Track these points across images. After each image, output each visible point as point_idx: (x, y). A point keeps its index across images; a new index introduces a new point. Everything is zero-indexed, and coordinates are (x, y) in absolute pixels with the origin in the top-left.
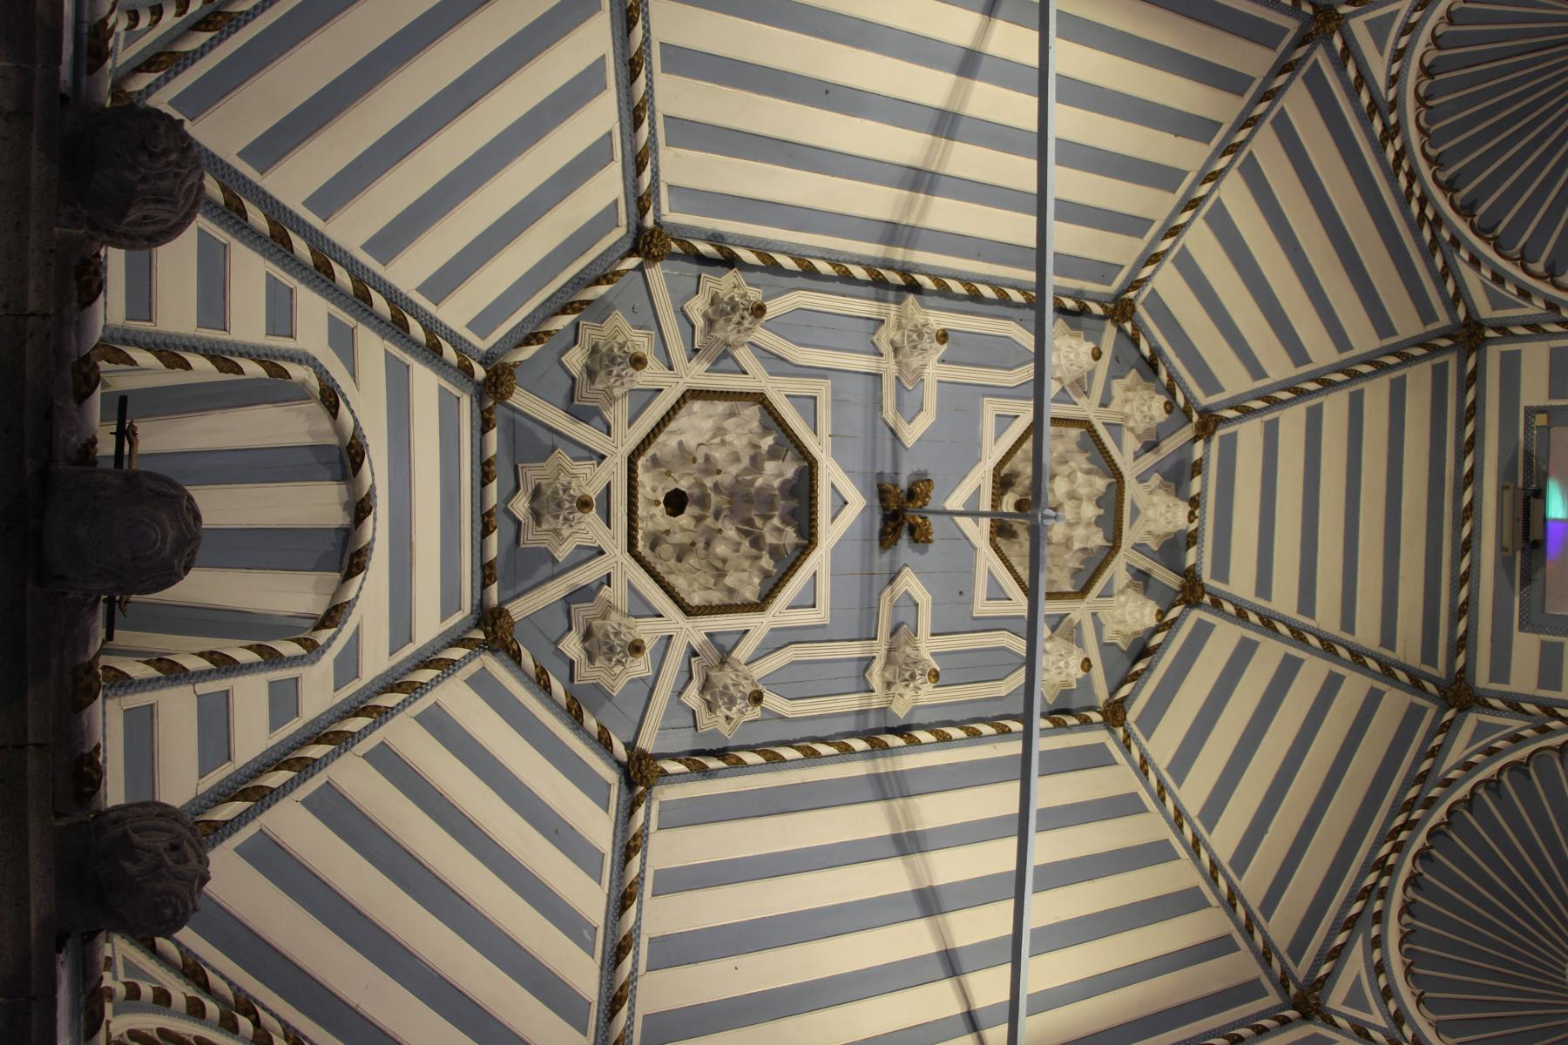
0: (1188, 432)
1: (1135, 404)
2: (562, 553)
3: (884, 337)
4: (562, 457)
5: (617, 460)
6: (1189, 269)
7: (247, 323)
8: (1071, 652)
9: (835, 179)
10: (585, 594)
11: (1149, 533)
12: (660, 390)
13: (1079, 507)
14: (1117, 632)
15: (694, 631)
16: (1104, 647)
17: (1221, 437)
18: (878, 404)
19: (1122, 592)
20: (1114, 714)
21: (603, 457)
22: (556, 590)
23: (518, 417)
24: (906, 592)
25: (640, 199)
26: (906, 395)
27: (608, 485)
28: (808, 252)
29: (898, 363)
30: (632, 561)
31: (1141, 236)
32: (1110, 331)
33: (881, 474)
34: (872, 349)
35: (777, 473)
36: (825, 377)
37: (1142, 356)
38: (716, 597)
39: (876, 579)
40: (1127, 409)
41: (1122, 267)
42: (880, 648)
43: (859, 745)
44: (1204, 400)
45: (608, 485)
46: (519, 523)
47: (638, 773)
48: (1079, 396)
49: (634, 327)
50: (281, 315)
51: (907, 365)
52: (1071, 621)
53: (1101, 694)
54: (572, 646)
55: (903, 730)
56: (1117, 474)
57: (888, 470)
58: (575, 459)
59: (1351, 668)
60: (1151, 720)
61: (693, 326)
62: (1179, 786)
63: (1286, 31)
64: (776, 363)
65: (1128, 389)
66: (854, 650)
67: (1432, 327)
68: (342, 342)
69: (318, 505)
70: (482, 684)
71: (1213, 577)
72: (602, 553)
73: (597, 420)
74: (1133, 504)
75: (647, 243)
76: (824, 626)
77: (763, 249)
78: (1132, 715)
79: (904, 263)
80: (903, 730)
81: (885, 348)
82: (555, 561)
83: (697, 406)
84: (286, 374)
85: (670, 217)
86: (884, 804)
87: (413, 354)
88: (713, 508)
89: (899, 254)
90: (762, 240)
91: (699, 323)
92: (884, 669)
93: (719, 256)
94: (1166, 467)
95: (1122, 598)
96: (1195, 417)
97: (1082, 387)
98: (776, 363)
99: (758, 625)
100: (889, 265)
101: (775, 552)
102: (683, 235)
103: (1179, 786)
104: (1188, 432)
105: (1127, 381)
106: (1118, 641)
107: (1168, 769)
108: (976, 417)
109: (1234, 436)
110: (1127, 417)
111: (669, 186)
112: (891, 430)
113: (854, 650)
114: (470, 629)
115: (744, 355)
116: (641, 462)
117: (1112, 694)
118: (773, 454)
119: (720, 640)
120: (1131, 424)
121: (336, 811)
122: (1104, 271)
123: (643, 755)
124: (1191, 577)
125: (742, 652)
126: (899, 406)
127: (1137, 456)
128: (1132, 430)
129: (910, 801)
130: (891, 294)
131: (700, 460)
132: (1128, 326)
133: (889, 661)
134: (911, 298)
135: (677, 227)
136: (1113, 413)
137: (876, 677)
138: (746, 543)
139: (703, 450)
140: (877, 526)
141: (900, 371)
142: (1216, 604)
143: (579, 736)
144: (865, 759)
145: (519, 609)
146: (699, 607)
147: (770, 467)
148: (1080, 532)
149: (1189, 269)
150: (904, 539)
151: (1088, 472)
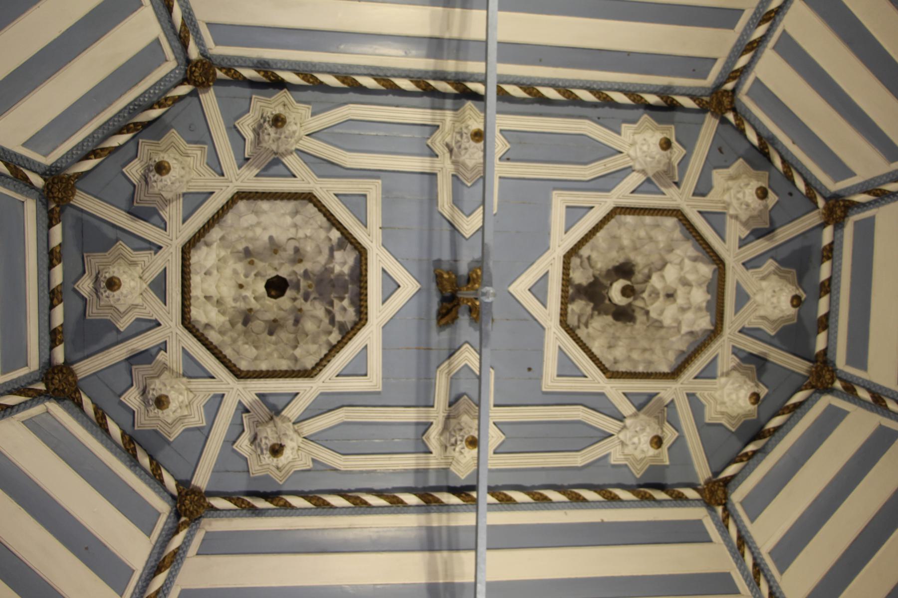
0: (813, 219)
1: (732, 192)
2: (123, 325)
3: (438, 142)
4: (122, 247)
5: (172, 250)
6: (792, 52)
8: (643, 430)
10: (144, 357)
12: (212, 193)
13: (689, 293)
14: (722, 413)
15: (247, 391)
16: (703, 427)
17: (856, 223)
19: (727, 374)
20: (716, 493)
21: (160, 248)
22: (119, 353)
23: (85, 216)
24: (466, 365)
25: (180, 37)
26: (466, 191)
28: (351, 71)
29: (455, 163)
30: (186, 332)
31: (732, 27)
32: (710, 124)
34: (427, 151)
35: (343, 263)
36: (378, 178)
37: (752, 145)
38: (284, 365)
39: (434, 355)
40: (726, 198)
41: (715, 60)
42: (438, 414)
43: (411, 499)
44: (834, 186)
46: (84, 300)
47: (189, 505)
48: (668, 186)
49: (189, 142)
51: (464, 165)
52: (661, 399)
53: (703, 472)
54: (132, 398)
55: (464, 491)
56: (718, 262)
57: (446, 256)
58: (135, 250)
60: (758, 503)
61: (245, 140)
62: (782, 572)
64: (325, 167)
65: (732, 178)
66: (411, 415)
71: (849, 362)
72: (159, 325)
73: (156, 219)
75: (200, 73)
76: (378, 393)
77: (306, 72)
78: (737, 496)
79: (457, 73)
80: (464, 491)
81: (439, 148)
82: (118, 331)
83: (242, 205)
85: (216, 50)
86: (427, 555)
88: (302, 291)
89: (450, 66)
90: (306, 64)
91: (249, 136)
92: (441, 434)
93: (264, 79)
94: (784, 253)
95: (723, 380)
96: (821, 203)
97: (672, 177)
98: (325, 167)
99: (308, 390)
100: (441, 76)
101: (342, 327)
103: (782, 572)
105: (731, 170)
106: (724, 422)
107: (771, 553)
110: (728, 205)
111: (208, 24)
112: (449, 222)
113: (411, 415)
114: (36, 381)
115: (293, 162)
116: (575, 261)
117: (716, 474)
118: (341, 246)
119: (271, 400)
120: (731, 211)
122: (697, 65)
123: (196, 491)
124: (823, 364)
125: (293, 411)
126: (456, 201)
128: (736, 217)
129: (455, 555)
130: (449, 102)
131: (291, 252)
132: (730, 116)
133: (446, 428)
134: (469, 104)
135: (223, 57)
136: (712, 201)
137: (433, 437)
138: (326, 321)
139: (293, 244)
141: (457, 170)
142: (849, 390)
143: (135, 472)
144: (418, 512)
145: (84, 369)
147: (338, 255)
148: (689, 315)
149: (792, 52)
150: (464, 320)
151: (695, 260)
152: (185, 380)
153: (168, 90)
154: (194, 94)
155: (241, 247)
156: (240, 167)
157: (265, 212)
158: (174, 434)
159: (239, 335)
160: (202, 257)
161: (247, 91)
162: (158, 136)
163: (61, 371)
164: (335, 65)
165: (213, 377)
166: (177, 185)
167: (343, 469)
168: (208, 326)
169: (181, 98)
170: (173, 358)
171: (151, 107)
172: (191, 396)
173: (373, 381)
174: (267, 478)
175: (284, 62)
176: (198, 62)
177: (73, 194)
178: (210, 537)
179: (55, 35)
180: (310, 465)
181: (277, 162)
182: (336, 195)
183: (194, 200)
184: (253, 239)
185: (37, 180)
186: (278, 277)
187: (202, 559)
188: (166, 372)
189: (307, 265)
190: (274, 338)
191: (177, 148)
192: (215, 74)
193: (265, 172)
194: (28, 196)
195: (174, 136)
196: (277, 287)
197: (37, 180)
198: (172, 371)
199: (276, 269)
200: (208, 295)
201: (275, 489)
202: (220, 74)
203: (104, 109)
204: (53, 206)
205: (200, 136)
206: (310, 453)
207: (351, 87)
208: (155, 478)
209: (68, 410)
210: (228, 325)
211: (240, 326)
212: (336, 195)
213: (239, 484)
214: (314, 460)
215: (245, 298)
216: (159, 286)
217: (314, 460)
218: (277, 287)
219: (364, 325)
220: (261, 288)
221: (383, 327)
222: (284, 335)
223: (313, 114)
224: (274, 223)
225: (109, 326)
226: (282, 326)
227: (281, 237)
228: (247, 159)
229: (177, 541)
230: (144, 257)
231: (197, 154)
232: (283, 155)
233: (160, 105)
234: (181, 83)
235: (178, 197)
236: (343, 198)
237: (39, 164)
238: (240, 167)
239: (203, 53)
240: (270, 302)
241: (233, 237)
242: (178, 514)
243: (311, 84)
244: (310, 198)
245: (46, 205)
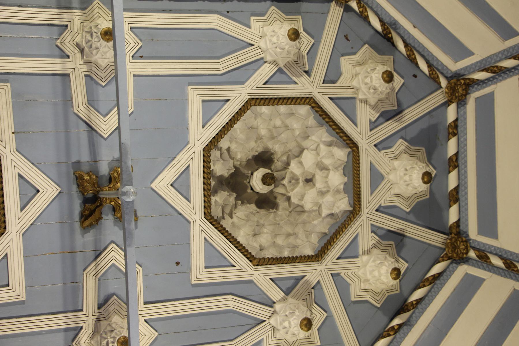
0: (438, 98)
10: (388, 116)
11: (397, 195)
16: (349, 305)
18: (67, 99)
22: (411, 114)
27: (356, 125)
33: (78, 162)
34: (57, 52)
36: (6, 81)
39: (79, 257)
40: (355, 83)
45: (356, 125)
56: (351, 144)
57: (85, 157)
65: (359, 64)
66: (59, 322)
71: (480, 232)
74: (372, 168)
76: (23, 302)
81: (69, 48)
94: (412, 133)
95: (365, 258)
96: (444, 83)
97: (302, 67)
98: (246, 290)
104: (438, 98)
105: (358, 57)
108: (182, 104)
109: (490, 98)
110: (356, 90)
113: (59, 322)
115: (275, 293)
120: (361, 96)
124: (457, 234)
125: (266, 71)
126: (92, 102)
127: (374, 125)
128: (366, 102)
136: (342, 87)
140: (77, 209)
142: (483, 257)
148: (329, 198)
150: (108, 220)
151: (330, 144)
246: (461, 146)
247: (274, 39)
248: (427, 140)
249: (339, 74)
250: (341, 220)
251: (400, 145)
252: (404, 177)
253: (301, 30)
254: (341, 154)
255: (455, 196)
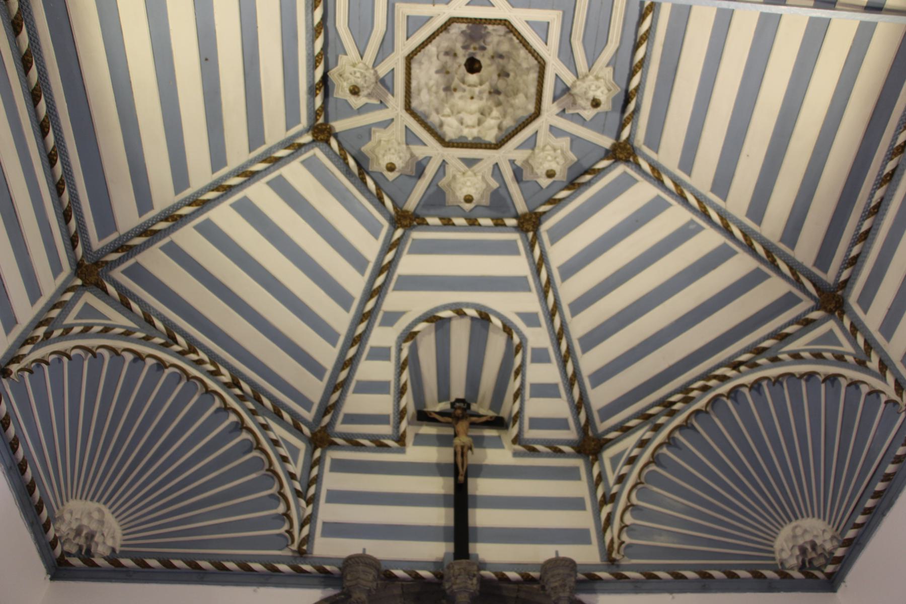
5: (445, 153)
7: (384, 371)
9: (259, 25)
10: (518, 174)
15: (550, 108)
21: (444, 161)
22: (514, 188)
47: (622, 152)
49: (370, 139)
50: (380, 354)
59: (577, 429)
63: (124, 272)
64: (386, 46)
67: (341, 417)
68: (391, 319)
69: (460, 333)
70: (557, 234)
73: (424, 163)
75: (321, 132)
77: (314, 62)
83: (414, 104)
84: (406, 360)
85: (304, 122)
87: (393, 275)
90: (308, 61)
93: (322, 90)
94: (503, 192)
98: (386, 46)
99: (555, 67)
102: (314, 115)
111: (288, 129)
115: (382, 70)
119: (558, 92)
121: (592, 339)
125: (568, 78)
127: (512, 162)
131: (448, 59)
135: (309, 118)
139: (442, 56)
145: (521, 207)
146: (536, 108)
152: (537, 151)
153: (335, 153)
154: (336, 136)
155: (442, 94)
156: (387, 107)
157: (419, 84)
158: (573, 157)
159: (508, 101)
160: (451, 130)
161: (331, 100)
162: (367, 159)
163: (522, 223)
164: (307, 39)
165: (537, 132)
166: (401, 154)
167: (617, 45)
168: (500, 128)
169: (339, 144)
170: (520, 157)
171: (347, 164)
172: (548, 147)
173: (553, 17)
174: (614, 100)
175: (308, 50)
176: (313, 135)
177: (407, 212)
178: (648, 143)
179: (308, 226)
180: (610, 69)
181: (382, 81)
182: (408, 38)
183: (411, 138)
184: (437, 85)
185: (399, 233)
186: (465, 65)
187: (661, 151)
188: (530, 161)
189: (458, 47)
190: (512, 74)
191: (374, 148)
192: (321, 124)
193: (391, 90)
194: (409, 236)
195: (365, 149)
196: (473, 66)
197: (399, 233)
198: (530, 157)
199: (460, 66)
200: (476, 122)
201: (623, 94)
202: (321, 120)
203: (352, 193)
204: (415, 223)
205: (366, 132)
206: (601, 68)
207: (323, 28)
208: (598, 173)
209: (546, 219)
210: (500, 108)
211: (501, 97)
212: (408, 38)
213: (615, 118)
214: (608, 65)
215: (481, 92)
216: (470, 162)
217: (608, 65)
218: (473, 66)
219: (509, 23)
220: (473, 78)
221: (513, 7)
222: (510, 67)
223: (346, 54)
224: (427, 72)
225: (495, 194)
226: (504, 67)
227: (436, 64)
228: (381, 102)
229: (645, 166)
230: (450, 171)
231: (379, 135)
232: (377, 77)
233: (345, 159)
234: (329, 145)
235: (408, 148)
236: (410, 33)
237: (389, 230)
238: (387, 107)
239: (307, 131)
240: (484, 71)
241: (436, 102)
242: (627, 161)
243: (324, 58)
244: (409, 59)
245: (414, 226)
246: (486, 229)
247: (593, 87)
248: (498, 205)
249: (557, 136)
250: (438, 130)
251: (495, 184)
252: (470, 184)
253: (599, 109)
254: (491, 136)
255: (447, 223)
